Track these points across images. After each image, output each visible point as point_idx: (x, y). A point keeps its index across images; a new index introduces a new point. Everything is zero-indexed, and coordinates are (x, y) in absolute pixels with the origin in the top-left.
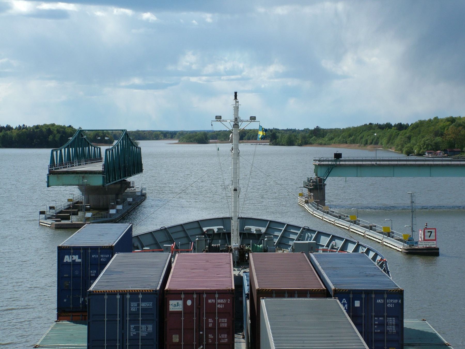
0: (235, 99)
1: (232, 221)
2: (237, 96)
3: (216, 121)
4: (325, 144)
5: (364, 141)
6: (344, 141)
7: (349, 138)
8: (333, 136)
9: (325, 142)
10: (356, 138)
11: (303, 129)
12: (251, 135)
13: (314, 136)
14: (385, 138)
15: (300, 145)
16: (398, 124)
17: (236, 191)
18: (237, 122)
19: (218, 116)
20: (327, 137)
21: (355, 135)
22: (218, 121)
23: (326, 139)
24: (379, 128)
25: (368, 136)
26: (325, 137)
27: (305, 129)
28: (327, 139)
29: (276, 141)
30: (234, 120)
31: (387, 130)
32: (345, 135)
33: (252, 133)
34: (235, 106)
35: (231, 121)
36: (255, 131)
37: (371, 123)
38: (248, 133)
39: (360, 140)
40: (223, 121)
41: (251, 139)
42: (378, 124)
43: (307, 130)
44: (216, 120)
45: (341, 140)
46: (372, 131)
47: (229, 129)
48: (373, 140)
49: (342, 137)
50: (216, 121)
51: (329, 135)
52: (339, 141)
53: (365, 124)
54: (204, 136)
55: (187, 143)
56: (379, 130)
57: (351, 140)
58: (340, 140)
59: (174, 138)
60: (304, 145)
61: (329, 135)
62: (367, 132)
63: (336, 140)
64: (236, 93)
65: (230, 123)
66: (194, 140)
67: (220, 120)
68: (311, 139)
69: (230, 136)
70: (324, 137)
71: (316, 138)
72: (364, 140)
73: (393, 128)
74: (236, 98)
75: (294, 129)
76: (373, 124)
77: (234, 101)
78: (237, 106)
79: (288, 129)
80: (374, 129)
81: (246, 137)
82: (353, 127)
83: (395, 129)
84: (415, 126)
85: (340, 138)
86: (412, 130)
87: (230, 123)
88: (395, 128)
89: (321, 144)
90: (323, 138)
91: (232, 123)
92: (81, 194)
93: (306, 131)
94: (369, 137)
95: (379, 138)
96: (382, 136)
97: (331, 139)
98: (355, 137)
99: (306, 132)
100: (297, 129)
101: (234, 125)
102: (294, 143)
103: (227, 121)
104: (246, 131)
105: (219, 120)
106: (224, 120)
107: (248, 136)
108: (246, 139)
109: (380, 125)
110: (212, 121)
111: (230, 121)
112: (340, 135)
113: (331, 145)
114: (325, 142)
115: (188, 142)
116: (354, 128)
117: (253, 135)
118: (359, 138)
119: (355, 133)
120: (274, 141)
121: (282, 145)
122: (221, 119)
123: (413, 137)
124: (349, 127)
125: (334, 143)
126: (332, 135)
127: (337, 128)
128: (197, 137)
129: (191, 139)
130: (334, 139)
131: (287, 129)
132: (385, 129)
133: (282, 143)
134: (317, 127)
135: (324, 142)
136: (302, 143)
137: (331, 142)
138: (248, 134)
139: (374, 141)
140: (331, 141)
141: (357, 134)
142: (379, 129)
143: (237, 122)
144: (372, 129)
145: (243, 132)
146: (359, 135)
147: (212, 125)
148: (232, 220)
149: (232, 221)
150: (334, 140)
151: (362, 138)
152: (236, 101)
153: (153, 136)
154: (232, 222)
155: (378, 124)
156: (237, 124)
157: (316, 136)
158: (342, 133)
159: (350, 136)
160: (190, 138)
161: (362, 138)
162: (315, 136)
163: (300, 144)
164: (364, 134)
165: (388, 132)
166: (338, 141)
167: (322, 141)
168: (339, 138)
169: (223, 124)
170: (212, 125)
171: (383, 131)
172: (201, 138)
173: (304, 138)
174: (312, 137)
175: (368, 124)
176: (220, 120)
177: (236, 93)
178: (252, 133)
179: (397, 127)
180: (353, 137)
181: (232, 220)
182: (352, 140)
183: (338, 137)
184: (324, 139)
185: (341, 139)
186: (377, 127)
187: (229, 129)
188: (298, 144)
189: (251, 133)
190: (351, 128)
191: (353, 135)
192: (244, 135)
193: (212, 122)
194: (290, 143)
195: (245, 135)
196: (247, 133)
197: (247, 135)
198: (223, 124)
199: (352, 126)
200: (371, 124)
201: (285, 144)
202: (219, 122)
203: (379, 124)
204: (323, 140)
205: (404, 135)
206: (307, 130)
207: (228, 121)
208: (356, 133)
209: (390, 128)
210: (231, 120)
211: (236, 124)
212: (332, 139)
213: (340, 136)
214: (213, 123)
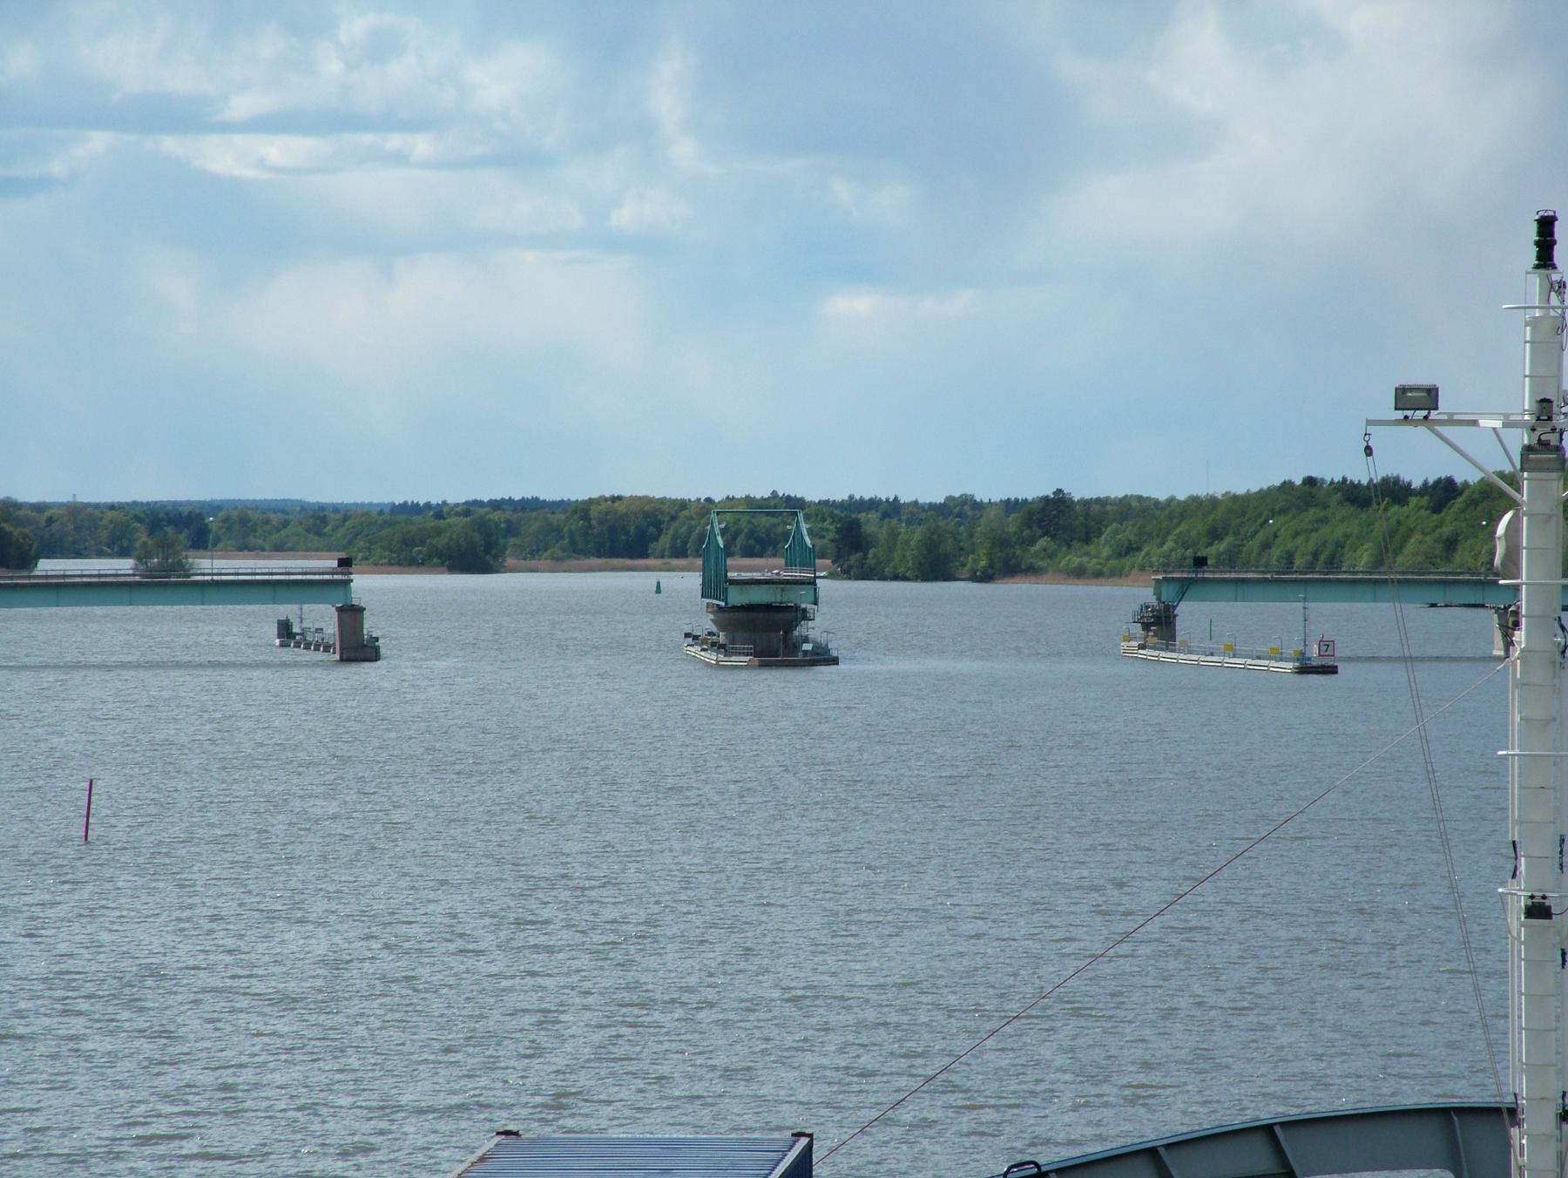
0: (1537, 267)
1: (1515, 1132)
2: (1554, 242)
3: (1397, 422)
4: (1098, 575)
5: (1280, 557)
6: (1185, 558)
7: (1210, 544)
8: (1132, 538)
9: (1101, 564)
10: (1243, 545)
11: (939, 499)
12: (690, 530)
13: (1041, 537)
14: (1366, 546)
15: (986, 577)
16: (1439, 481)
17: (1546, 922)
18: (1554, 430)
19: (1412, 389)
20: (1106, 540)
21: (1237, 533)
22: (1416, 423)
23: (1103, 548)
24: (1348, 499)
25: (1296, 535)
26: (1095, 540)
27: (950, 499)
28: (1106, 552)
29: (866, 559)
30: (1527, 417)
31: (1385, 510)
32: (1193, 533)
33: (693, 523)
34: (1538, 313)
35: (1505, 425)
36: (323, 520)
37: (1314, 474)
38: (673, 518)
39: (1260, 554)
40: (1451, 422)
41: (689, 552)
42: (1345, 479)
43: (966, 508)
44: (1400, 415)
45: (1173, 555)
46: (1313, 513)
47: (1480, 468)
48: (1316, 555)
49: (1176, 542)
50: (1397, 422)
51: (1116, 532)
52: (1162, 560)
53: (1284, 483)
54: (477, 536)
55: (390, 568)
56: (1348, 509)
57: (1219, 554)
58: (1167, 556)
59: (215, 545)
60: (999, 579)
61: (1116, 532)
62: (1294, 517)
63: (1148, 554)
64: (1546, 225)
65: (1498, 436)
66: (430, 556)
67: (1425, 413)
68: (1032, 549)
69: (1501, 529)
70: (1087, 541)
71: (1053, 546)
72: (1275, 553)
73: (1413, 501)
74: (1551, 258)
75: (887, 500)
76: (1323, 481)
77: (1535, 280)
78: (1552, 313)
79: (858, 497)
80: (1325, 506)
81: (665, 541)
82: (1228, 493)
83: (1422, 507)
84: (1476, 496)
85: (1169, 544)
86: (1463, 511)
87: (1498, 436)
88: (1425, 501)
89: (1079, 573)
90: (1086, 548)
91: (1520, 439)
92: (1073, 1137)
93: (957, 510)
94: (1300, 540)
95: (1343, 547)
96: (1358, 538)
97: (1127, 553)
98: (1237, 543)
99: (959, 515)
100: (905, 498)
101: (1528, 449)
102: (953, 569)
103: (1475, 423)
104: (662, 513)
105: (1421, 414)
106: (1456, 417)
107: (675, 537)
108: (664, 551)
109: (1355, 487)
110: (1369, 423)
111: (1498, 424)
112: (1168, 533)
113: (1127, 576)
114: (1101, 564)
115: (399, 564)
116: (1235, 498)
117: (699, 528)
118: (1254, 544)
119: (1238, 520)
120: (854, 558)
121: (896, 577)
122: (1437, 408)
123: (1466, 539)
124: (1210, 493)
125: (1142, 568)
126: (1129, 533)
127: (1136, 493)
128: (441, 542)
129: (416, 549)
130: (1139, 549)
131: (851, 497)
132: (1375, 506)
133: (896, 568)
134: (1060, 491)
135: (1092, 564)
136: (991, 565)
137: (1128, 564)
138: (675, 525)
139: (1322, 558)
140: (1127, 561)
141: (1246, 529)
142: (1348, 503)
143: (1554, 430)
144: (1315, 506)
145: (647, 515)
146: (1256, 532)
147: (1369, 451)
148: (1516, 1122)
149: (1515, 1132)
150: (1143, 553)
151: (1266, 546)
152: (1548, 277)
153: (104, 535)
154: (1520, 1138)
155: (1345, 479)
156: (1553, 439)
157: (1054, 537)
158: (1179, 524)
159: (1215, 535)
160: (408, 542)
161: (1266, 546)
162: (1045, 534)
163: (983, 573)
164: (1279, 530)
165: (1385, 516)
166: (1158, 561)
167: (1085, 559)
168: (1162, 544)
169: (1451, 445)
170: (1369, 451)
171: (1364, 516)
172: (462, 542)
173: (1001, 543)
174: (1032, 541)
175: (1298, 482)
176: (1426, 418)
177: (1546, 225)
178: (693, 523)
179: (1431, 496)
180: (1229, 539)
181: (1516, 1122)
182: (1225, 556)
183: (1158, 541)
184: (1092, 548)
185: (1172, 550)
186: (1339, 494)
187: (1480, 468)
188: (975, 573)
189: (691, 518)
190: (1220, 497)
191: (1227, 534)
192: (652, 530)
193: (1371, 429)
194: (935, 567)
195: (660, 531)
196: (666, 519)
197: (671, 532)
198: (1451, 445)
199: (1224, 492)
200: (1310, 481)
201: (908, 575)
202: (1422, 429)
203: (1351, 481)
204: (1088, 554)
205: (1434, 531)
206: (966, 508)
207: (1483, 423)
208: (1242, 523)
209: (1399, 504)
210: (1507, 416)
211: (1543, 445)
212: (1130, 549)
213: (1169, 538)
214: (1379, 437)
